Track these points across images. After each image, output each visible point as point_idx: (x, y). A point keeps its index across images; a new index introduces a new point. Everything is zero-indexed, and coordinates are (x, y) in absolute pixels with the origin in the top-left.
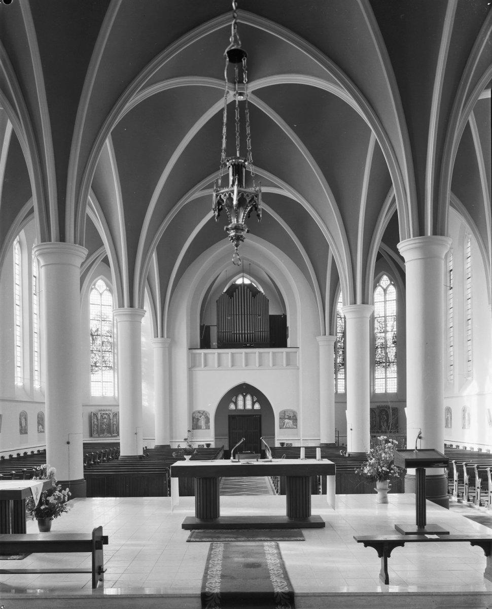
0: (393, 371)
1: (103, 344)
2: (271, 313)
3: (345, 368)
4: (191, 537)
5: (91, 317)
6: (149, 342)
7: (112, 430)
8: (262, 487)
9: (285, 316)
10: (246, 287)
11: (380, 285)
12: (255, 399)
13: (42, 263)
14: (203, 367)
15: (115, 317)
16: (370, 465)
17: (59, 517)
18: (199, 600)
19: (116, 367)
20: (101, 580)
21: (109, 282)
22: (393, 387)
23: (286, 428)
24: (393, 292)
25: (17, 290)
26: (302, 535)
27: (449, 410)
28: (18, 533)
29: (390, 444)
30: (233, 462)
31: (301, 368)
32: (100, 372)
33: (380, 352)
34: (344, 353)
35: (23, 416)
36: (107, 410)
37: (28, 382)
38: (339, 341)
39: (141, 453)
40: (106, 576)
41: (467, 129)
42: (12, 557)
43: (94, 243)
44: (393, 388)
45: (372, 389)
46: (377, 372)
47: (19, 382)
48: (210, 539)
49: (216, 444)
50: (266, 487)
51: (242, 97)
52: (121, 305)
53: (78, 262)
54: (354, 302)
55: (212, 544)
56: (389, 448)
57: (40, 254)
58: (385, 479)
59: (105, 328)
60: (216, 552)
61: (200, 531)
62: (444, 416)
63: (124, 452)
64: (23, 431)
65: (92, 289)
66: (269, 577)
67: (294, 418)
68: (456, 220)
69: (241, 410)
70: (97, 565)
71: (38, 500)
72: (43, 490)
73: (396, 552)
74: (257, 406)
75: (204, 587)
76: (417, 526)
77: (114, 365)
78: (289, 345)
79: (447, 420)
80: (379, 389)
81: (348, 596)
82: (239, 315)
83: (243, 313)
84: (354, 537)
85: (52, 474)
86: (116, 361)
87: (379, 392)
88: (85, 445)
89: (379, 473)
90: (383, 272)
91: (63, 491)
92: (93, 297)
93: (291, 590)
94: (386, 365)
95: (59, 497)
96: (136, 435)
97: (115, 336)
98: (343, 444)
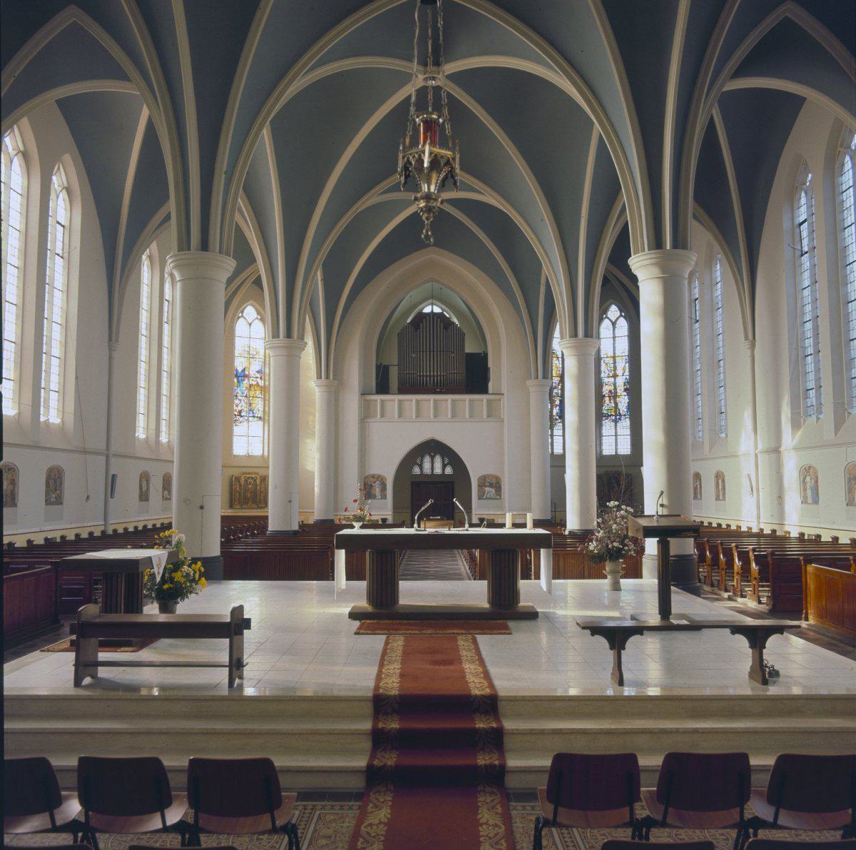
0: (625, 425)
1: (250, 387)
2: (467, 350)
3: (563, 422)
4: (360, 628)
5: (236, 354)
6: (312, 387)
7: (258, 500)
8: (456, 574)
9: (486, 355)
10: (435, 318)
11: (607, 317)
12: (446, 461)
13: (178, 277)
14: (379, 416)
15: (267, 351)
16: (597, 540)
17: (186, 600)
18: (370, 705)
19: (266, 418)
20: (241, 677)
21: (261, 310)
22: (625, 446)
23: (487, 498)
24: (623, 325)
25: (144, 317)
26: (507, 628)
27: (697, 476)
28: (132, 613)
29: (622, 512)
30: (417, 530)
31: (506, 420)
32: (245, 424)
33: (608, 405)
34: (562, 402)
35: (145, 477)
36: (252, 473)
37: (152, 432)
38: (555, 388)
39: (296, 528)
40: (247, 672)
41: (711, 126)
42: (123, 649)
43: (244, 256)
44: (625, 448)
45: (598, 449)
46: (604, 428)
47: (141, 434)
48: (386, 632)
49: (394, 520)
50: (460, 574)
51: (434, 82)
52: (275, 335)
53: (224, 276)
54: (575, 335)
55: (387, 637)
56: (623, 517)
57: (175, 267)
58: (617, 558)
59: (254, 368)
60: (392, 657)
61: (372, 621)
62: (692, 483)
63: (272, 526)
64: (144, 496)
65: (239, 317)
66: (464, 677)
67: (496, 485)
68: (700, 235)
69: (427, 475)
70: (235, 657)
71: (161, 575)
72: (167, 563)
73: (633, 641)
74: (449, 470)
75: (377, 687)
76: (659, 616)
77: (264, 416)
78: (490, 390)
79: (695, 489)
80: (608, 450)
81: (569, 700)
82: (426, 351)
83: (432, 350)
84: (577, 624)
85: (179, 543)
86: (267, 409)
87: (608, 454)
88: (224, 519)
89: (609, 551)
90: (611, 300)
91: (193, 565)
92: (241, 326)
93: (493, 693)
94: (616, 419)
95: (188, 574)
96: (289, 504)
97: (267, 378)
98: (561, 520)
